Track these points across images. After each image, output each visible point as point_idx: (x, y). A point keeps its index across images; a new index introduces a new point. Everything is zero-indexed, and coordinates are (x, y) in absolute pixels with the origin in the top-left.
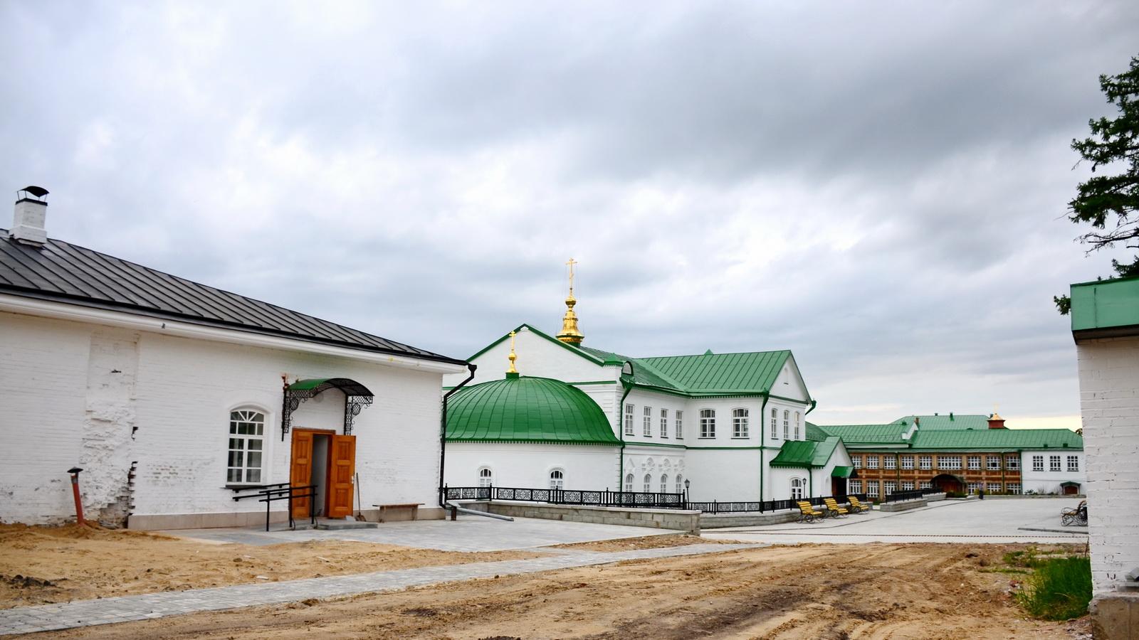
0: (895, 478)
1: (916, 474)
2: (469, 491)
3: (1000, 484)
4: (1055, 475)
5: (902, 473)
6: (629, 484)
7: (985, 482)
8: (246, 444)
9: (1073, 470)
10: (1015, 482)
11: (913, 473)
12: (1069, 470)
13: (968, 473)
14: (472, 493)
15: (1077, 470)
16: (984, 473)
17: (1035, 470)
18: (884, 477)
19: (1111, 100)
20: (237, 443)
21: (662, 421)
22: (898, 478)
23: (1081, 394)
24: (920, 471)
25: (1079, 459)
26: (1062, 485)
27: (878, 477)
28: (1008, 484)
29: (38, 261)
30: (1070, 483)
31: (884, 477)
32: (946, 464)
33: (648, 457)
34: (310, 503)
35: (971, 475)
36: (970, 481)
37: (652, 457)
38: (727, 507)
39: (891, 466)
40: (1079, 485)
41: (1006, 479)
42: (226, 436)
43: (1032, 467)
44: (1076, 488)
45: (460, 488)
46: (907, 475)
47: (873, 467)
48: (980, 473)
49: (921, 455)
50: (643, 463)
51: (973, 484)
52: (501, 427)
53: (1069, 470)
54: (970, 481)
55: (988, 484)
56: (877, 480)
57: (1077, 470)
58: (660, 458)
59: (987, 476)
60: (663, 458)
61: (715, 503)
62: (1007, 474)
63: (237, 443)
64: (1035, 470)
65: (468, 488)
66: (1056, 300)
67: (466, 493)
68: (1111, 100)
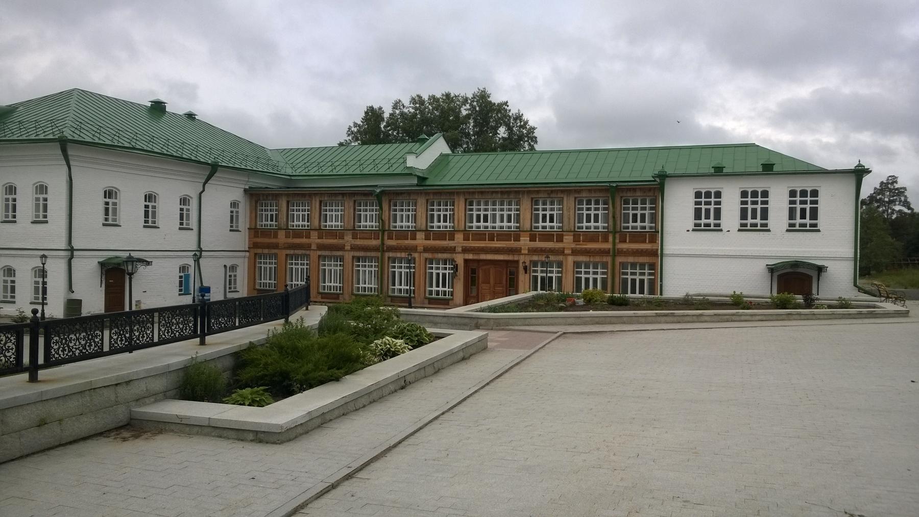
0: (375, 249)
1: (282, 237)
3: (604, 266)
4: (754, 243)
5: (390, 238)
6: (232, 274)
7: (348, 256)
9: (803, 228)
10: (642, 260)
11: (414, 238)
12: (791, 228)
13: (533, 239)
15: (814, 228)
16: (568, 239)
17: (697, 228)
18: (354, 248)
22: (382, 249)
24: (428, 234)
25: (821, 198)
26: (772, 270)
27: (341, 248)
28: (624, 265)
30: (796, 264)
31: (354, 248)
32: (486, 217)
34: (863, 299)
35: (538, 244)
36: (535, 258)
39: (505, 224)
40: (820, 269)
41: (621, 253)
42: (229, 209)
43: (690, 222)
44: (810, 278)
46: (267, 240)
47: (298, 224)
48: (560, 239)
49: (357, 198)
51: (587, 266)
52: (627, 189)
53: (791, 228)
54: (535, 258)
55: (577, 265)
56: (274, 251)
57: (814, 228)
59: (573, 246)
62: (623, 241)
64: (697, 228)
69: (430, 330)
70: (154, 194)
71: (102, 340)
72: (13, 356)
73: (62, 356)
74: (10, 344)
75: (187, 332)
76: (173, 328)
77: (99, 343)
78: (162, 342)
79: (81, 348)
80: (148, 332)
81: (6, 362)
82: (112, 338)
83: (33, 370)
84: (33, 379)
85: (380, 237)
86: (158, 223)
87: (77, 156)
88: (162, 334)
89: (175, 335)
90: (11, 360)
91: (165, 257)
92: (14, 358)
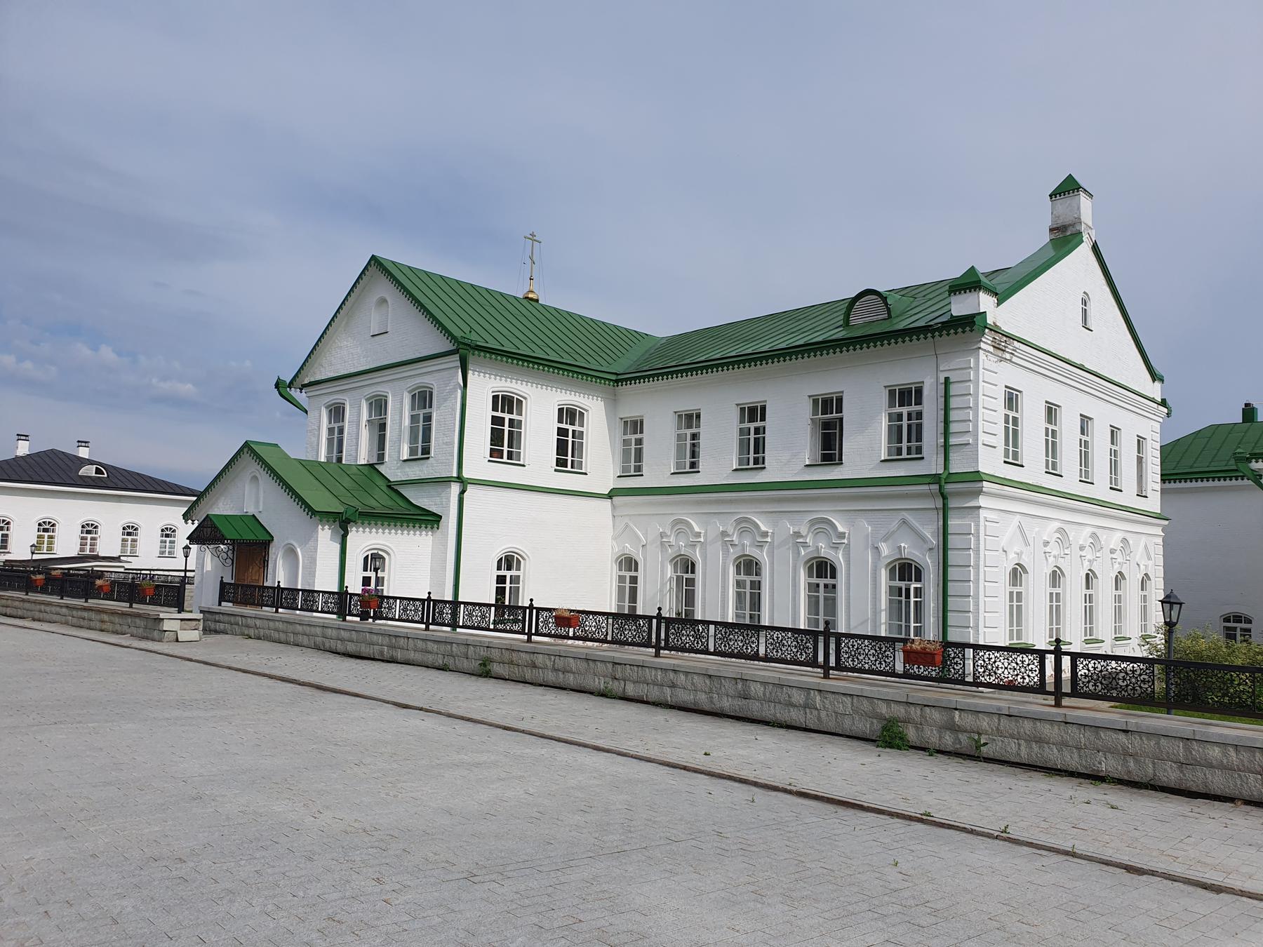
2: (476, 620)
8: (905, 417)
14: (470, 615)
19: (187, 523)
20: (914, 415)
21: (1007, 421)
23: (739, 458)
29: (318, 378)
33: (1057, 525)
37: (1066, 527)
38: (621, 629)
45: (395, 598)
50: (1112, 547)
58: (1083, 527)
60: (1118, 536)
61: (531, 607)
63: (914, 415)
65: (409, 599)
66: (998, 305)
67: (405, 610)
68: (187, 523)
69: (334, 616)
70: (516, 396)
71: (400, 607)
72: (1036, 678)
73: (852, 665)
74: (1090, 666)
75: (286, 592)
76: (480, 614)
77: (1086, 687)
78: (767, 659)
79: (870, 664)
80: (754, 646)
81: (979, 672)
82: (977, 670)
83: (658, 648)
84: (826, 676)
85: (838, 427)
86: (586, 467)
87: (410, 376)
88: (769, 651)
89: (627, 639)
90: (1123, 692)
91: (1076, 495)
92: (1124, 695)
